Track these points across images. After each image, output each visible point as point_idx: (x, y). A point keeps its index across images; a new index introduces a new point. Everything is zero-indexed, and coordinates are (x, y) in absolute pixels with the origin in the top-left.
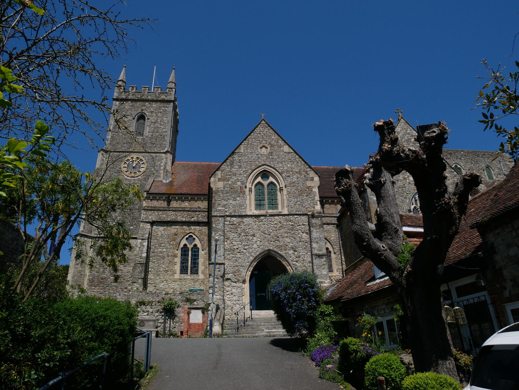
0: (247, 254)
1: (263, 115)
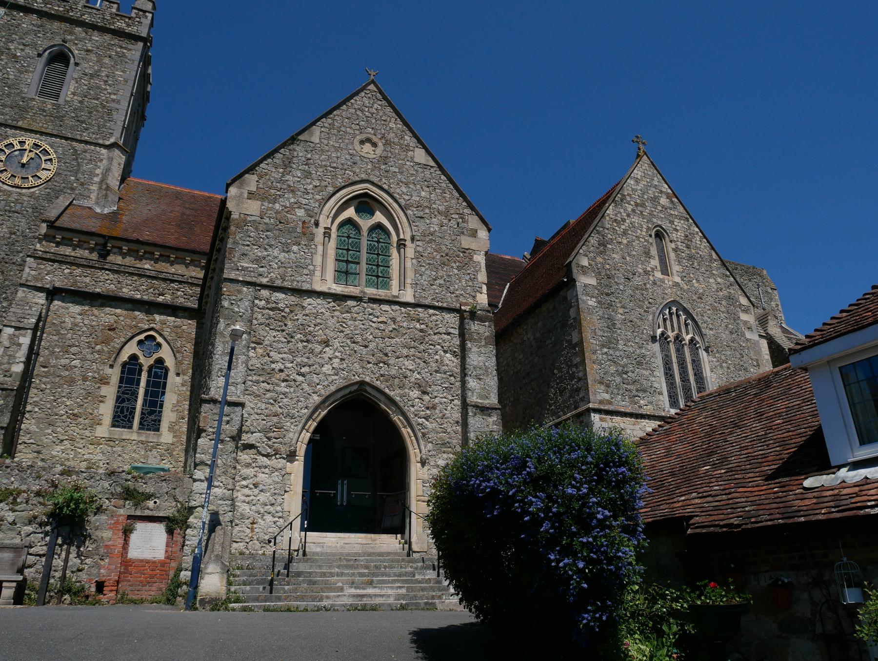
0: (305, 386)
1: (373, 73)
